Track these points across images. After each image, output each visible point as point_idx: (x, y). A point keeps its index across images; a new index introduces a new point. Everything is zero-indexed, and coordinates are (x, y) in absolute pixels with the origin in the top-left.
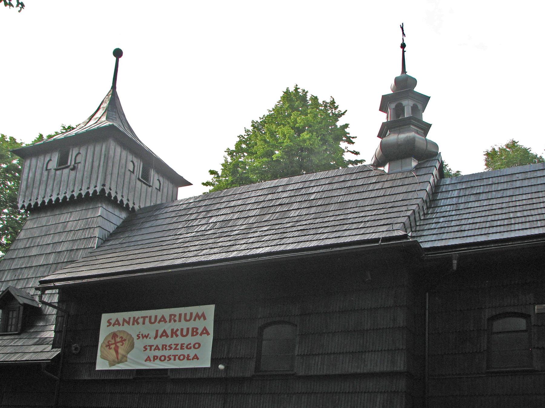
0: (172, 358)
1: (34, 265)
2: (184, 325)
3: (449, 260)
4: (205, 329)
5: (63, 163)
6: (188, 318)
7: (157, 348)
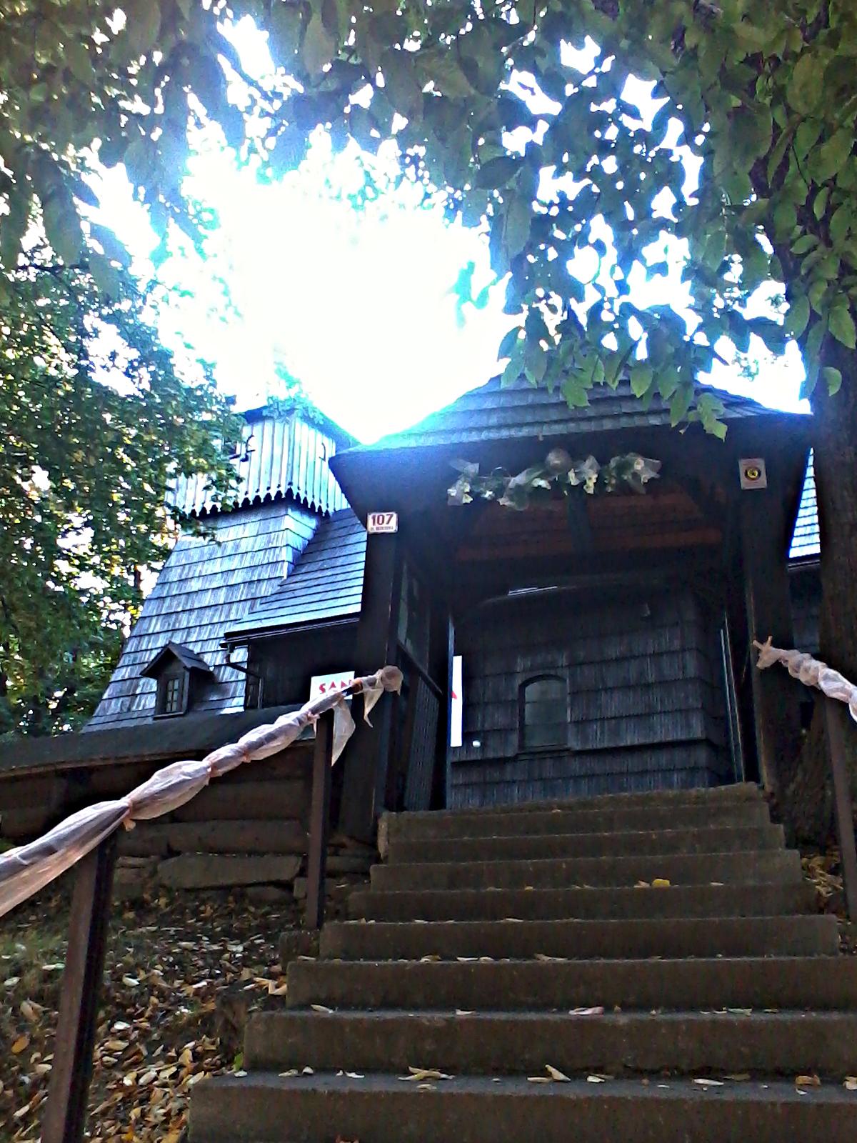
1: (196, 606)
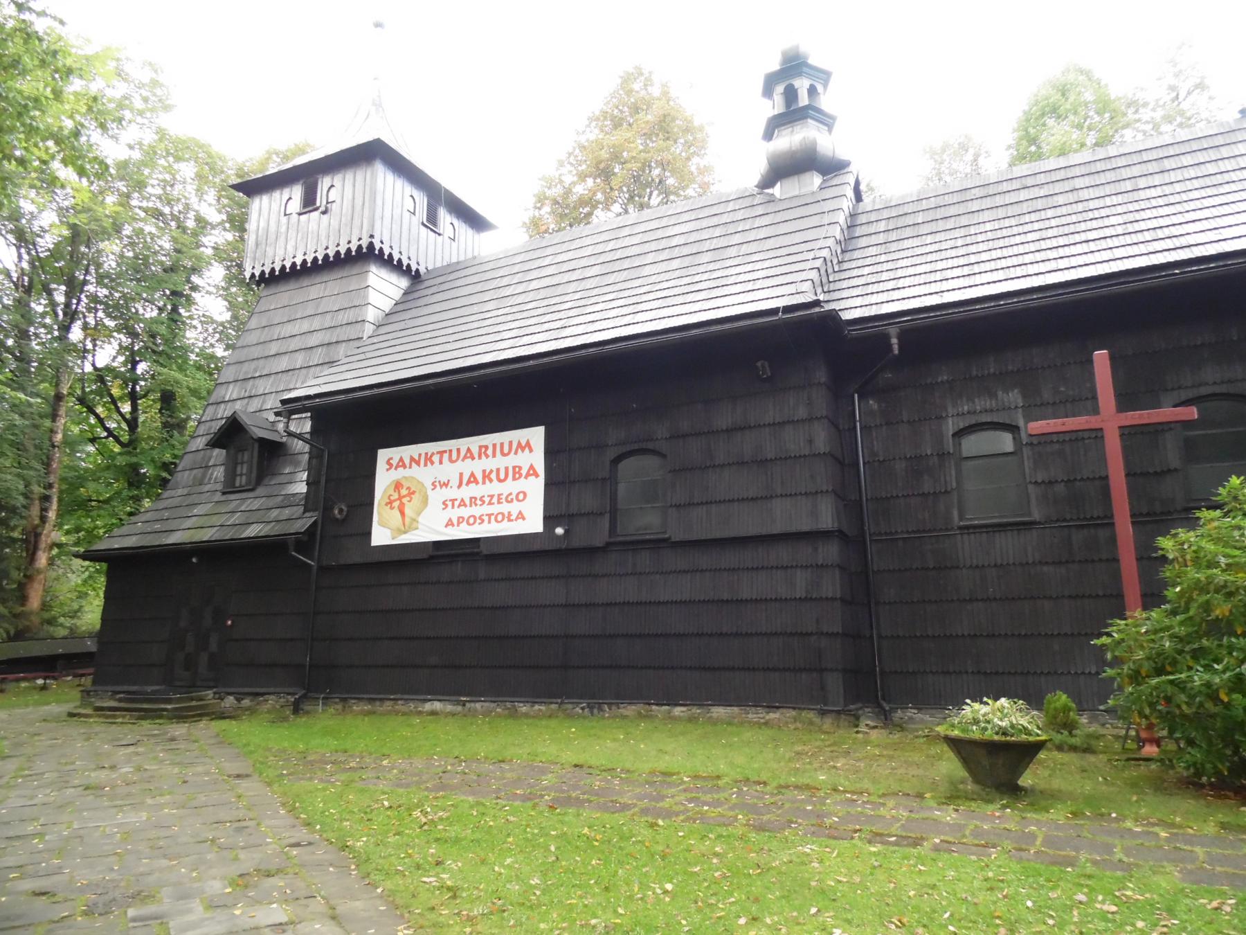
0: (486, 518)
2: (499, 462)
3: (885, 337)
4: (532, 467)
5: (309, 201)
6: (506, 451)
7: (463, 504)
